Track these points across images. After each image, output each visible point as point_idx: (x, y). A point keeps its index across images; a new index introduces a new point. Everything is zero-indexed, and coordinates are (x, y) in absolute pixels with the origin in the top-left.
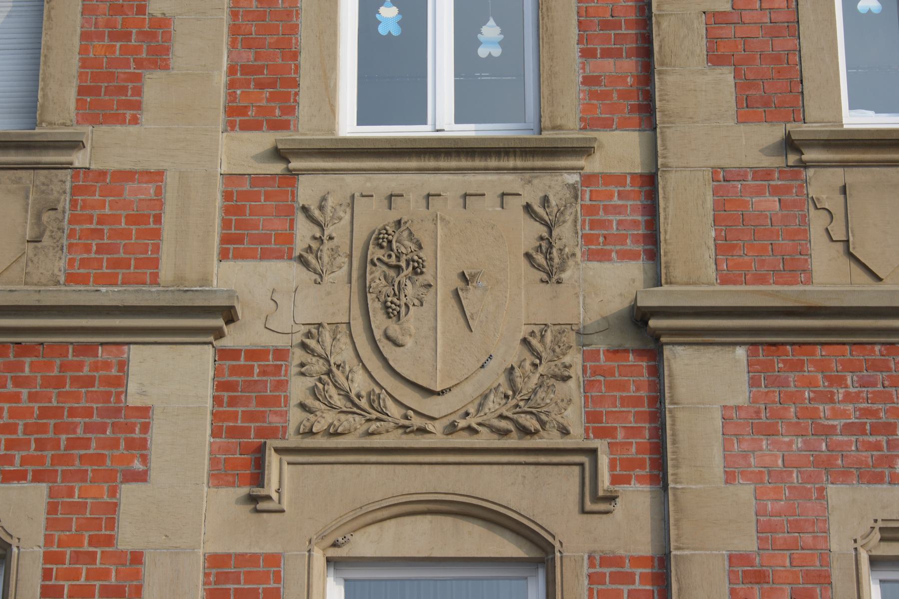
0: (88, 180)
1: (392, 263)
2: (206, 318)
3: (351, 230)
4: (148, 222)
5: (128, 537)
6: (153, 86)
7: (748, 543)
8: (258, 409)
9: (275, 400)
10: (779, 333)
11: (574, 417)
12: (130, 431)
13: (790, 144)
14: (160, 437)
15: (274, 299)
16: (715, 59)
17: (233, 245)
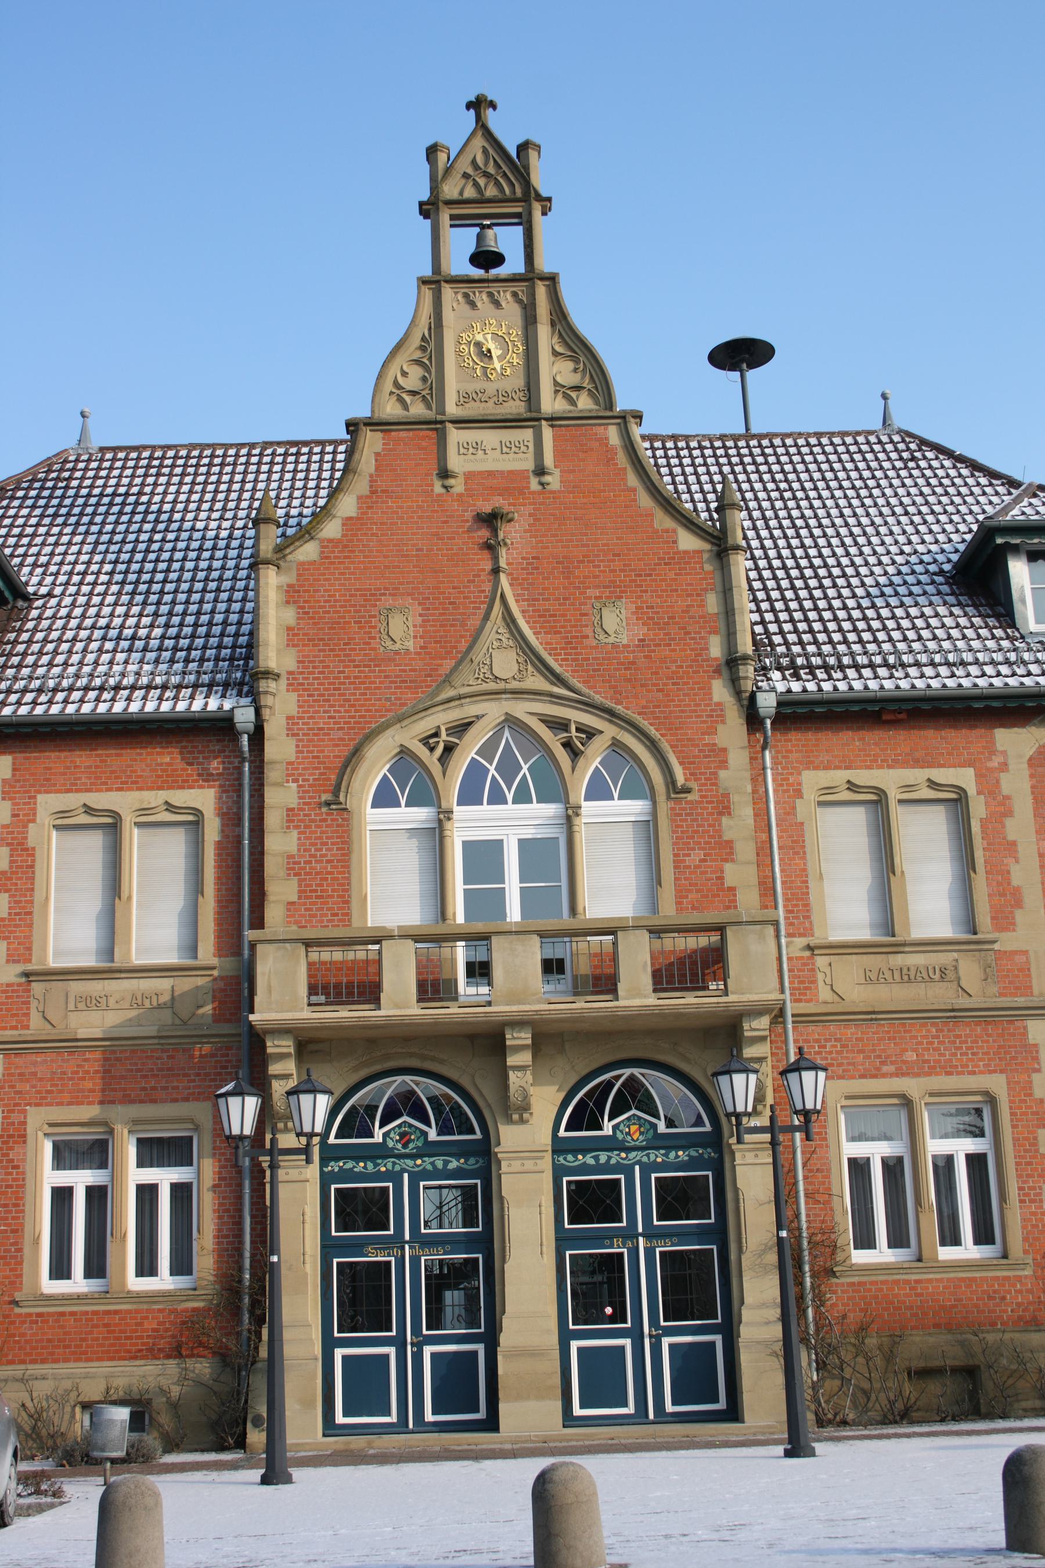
0: (1000, 954)
6: (1019, 915)
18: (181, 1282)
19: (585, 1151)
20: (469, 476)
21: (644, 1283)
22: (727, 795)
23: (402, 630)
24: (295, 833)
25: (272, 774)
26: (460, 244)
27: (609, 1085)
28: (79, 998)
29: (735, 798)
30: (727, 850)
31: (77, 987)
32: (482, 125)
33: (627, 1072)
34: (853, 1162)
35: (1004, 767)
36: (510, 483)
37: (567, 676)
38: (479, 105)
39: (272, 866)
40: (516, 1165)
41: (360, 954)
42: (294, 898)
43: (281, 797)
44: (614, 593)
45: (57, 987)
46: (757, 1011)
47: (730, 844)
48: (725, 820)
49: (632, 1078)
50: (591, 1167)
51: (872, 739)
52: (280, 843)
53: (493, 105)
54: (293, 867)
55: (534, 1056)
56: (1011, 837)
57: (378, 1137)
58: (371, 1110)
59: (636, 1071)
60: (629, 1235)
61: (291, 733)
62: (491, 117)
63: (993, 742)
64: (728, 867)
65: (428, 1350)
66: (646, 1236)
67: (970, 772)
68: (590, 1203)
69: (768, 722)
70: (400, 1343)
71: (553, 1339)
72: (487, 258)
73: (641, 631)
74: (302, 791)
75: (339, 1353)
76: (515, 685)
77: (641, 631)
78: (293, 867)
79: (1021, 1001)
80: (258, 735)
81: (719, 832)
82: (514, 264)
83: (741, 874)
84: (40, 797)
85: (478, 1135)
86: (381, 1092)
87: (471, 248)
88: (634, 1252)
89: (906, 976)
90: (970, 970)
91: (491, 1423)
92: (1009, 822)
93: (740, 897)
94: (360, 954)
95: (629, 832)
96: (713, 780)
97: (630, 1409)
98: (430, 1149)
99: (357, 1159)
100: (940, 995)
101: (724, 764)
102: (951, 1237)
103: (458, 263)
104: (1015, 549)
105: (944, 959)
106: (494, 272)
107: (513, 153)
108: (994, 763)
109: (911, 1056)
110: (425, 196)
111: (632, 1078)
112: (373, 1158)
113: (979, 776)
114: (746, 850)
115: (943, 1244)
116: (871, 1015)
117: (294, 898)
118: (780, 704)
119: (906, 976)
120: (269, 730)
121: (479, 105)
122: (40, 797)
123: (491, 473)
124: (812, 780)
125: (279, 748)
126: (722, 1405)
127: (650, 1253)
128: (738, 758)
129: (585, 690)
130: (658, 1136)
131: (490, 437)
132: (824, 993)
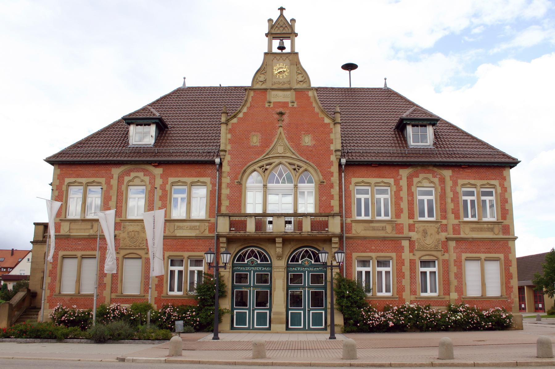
0: (397, 224)
1: (425, 232)
2: (409, 238)
3: (421, 229)
4: (402, 228)
5: (403, 258)
6: (402, 215)
7: (455, 258)
8: (397, 235)
9: (414, 245)
10: (459, 240)
11: (441, 247)
12: (403, 248)
13: (460, 222)
14: (405, 249)
15: (414, 235)
16: (452, 213)
17: (410, 230)
18: (180, 293)
19: (294, 267)
20: (274, 103)
21: (252, 299)
22: (333, 184)
23: (255, 140)
24: (229, 189)
25: (224, 175)
26: (276, 43)
27: (247, 251)
28: (178, 227)
29: (335, 184)
30: (332, 197)
31: (177, 224)
32: (282, 15)
33: (305, 249)
34: (378, 272)
35: (401, 179)
36: (285, 105)
37: (296, 153)
38: (282, 9)
39: (223, 197)
40: (278, 270)
41: (243, 218)
42: (228, 205)
43: (226, 180)
44: (308, 132)
45: (172, 224)
46: (335, 236)
47: (333, 195)
48: (332, 190)
49: (307, 250)
50: (295, 270)
51: (371, 170)
52: (225, 191)
53: (285, 9)
54: (228, 197)
55: (283, 245)
56: (401, 196)
57: (246, 262)
58: (245, 255)
59: (254, 248)
60: (304, 287)
61: (229, 165)
62: (285, 13)
63: (399, 172)
64: (332, 201)
65: (256, 311)
66: (308, 287)
67: (393, 180)
68: (296, 278)
69: (343, 166)
70: (304, 310)
71: (284, 310)
72: (281, 48)
73: (314, 143)
74: (231, 179)
75: (290, 312)
76: (283, 155)
77: (314, 143)
78: (228, 197)
79: (401, 235)
80: (221, 164)
81: (330, 192)
82: (288, 50)
83: (335, 203)
84: (169, 178)
85: (270, 262)
86: (247, 251)
87: (278, 45)
88: (250, 291)
89: (374, 229)
90: (389, 228)
91: (269, 329)
92: (401, 192)
93: (334, 209)
94: (243, 218)
95: (45, 202)
96: (330, 180)
97: (302, 327)
98: (258, 265)
99: (241, 267)
100: (381, 234)
101: (332, 176)
102: (172, 289)
103: (275, 50)
104: (409, 124)
105: (383, 225)
106: (284, 51)
107: (289, 22)
108: (399, 177)
109: (373, 248)
110: (267, 32)
111: (307, 250)
112: (245, 267)
113: (395, 181)
114: (337, 197)
115: (422, 292)
116: (365, 238)
117: (228, 205)
118: (346, 162)
119: (374, 229)
120: (223, 164)
121: (282, 9)
122: (169, 178)
123: (279, 102)
124: (354, 180)
125: (226, 168)
126: (268, 326)
127: (308, 292)
128: (336, 174)
129: (298, 156)
130: (312, 264)
131: (280, 93)
132: (354, 232)
